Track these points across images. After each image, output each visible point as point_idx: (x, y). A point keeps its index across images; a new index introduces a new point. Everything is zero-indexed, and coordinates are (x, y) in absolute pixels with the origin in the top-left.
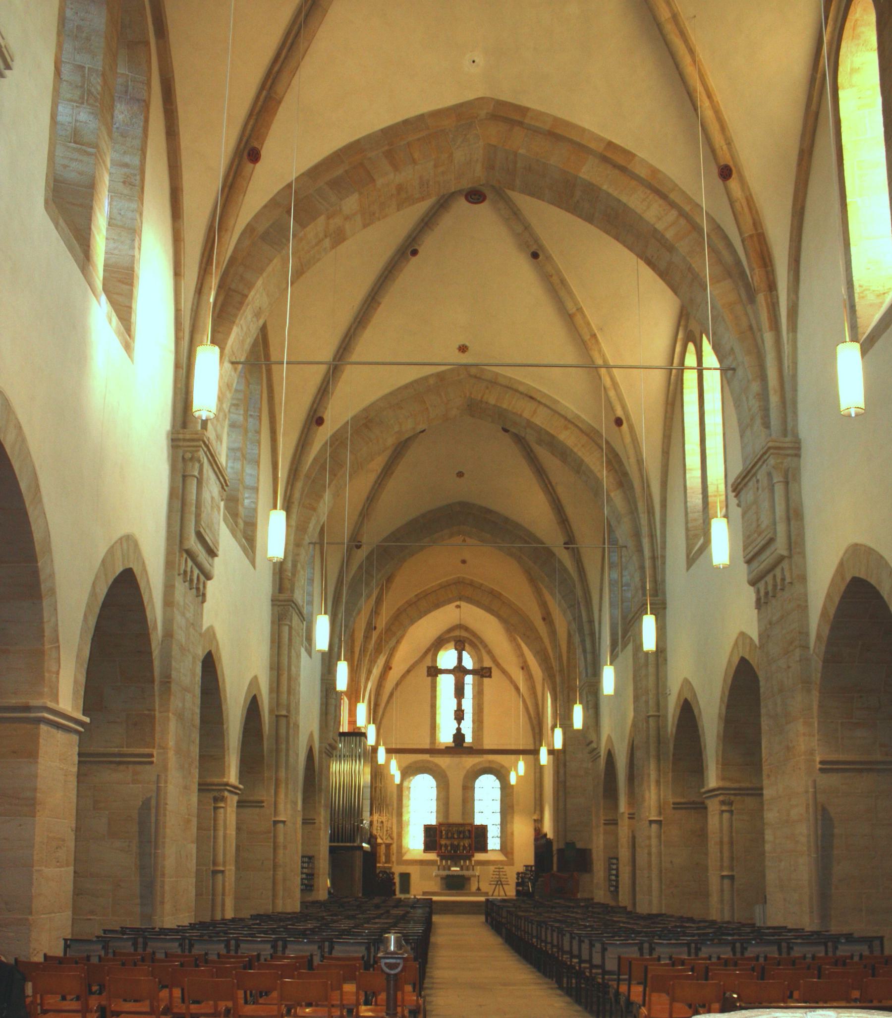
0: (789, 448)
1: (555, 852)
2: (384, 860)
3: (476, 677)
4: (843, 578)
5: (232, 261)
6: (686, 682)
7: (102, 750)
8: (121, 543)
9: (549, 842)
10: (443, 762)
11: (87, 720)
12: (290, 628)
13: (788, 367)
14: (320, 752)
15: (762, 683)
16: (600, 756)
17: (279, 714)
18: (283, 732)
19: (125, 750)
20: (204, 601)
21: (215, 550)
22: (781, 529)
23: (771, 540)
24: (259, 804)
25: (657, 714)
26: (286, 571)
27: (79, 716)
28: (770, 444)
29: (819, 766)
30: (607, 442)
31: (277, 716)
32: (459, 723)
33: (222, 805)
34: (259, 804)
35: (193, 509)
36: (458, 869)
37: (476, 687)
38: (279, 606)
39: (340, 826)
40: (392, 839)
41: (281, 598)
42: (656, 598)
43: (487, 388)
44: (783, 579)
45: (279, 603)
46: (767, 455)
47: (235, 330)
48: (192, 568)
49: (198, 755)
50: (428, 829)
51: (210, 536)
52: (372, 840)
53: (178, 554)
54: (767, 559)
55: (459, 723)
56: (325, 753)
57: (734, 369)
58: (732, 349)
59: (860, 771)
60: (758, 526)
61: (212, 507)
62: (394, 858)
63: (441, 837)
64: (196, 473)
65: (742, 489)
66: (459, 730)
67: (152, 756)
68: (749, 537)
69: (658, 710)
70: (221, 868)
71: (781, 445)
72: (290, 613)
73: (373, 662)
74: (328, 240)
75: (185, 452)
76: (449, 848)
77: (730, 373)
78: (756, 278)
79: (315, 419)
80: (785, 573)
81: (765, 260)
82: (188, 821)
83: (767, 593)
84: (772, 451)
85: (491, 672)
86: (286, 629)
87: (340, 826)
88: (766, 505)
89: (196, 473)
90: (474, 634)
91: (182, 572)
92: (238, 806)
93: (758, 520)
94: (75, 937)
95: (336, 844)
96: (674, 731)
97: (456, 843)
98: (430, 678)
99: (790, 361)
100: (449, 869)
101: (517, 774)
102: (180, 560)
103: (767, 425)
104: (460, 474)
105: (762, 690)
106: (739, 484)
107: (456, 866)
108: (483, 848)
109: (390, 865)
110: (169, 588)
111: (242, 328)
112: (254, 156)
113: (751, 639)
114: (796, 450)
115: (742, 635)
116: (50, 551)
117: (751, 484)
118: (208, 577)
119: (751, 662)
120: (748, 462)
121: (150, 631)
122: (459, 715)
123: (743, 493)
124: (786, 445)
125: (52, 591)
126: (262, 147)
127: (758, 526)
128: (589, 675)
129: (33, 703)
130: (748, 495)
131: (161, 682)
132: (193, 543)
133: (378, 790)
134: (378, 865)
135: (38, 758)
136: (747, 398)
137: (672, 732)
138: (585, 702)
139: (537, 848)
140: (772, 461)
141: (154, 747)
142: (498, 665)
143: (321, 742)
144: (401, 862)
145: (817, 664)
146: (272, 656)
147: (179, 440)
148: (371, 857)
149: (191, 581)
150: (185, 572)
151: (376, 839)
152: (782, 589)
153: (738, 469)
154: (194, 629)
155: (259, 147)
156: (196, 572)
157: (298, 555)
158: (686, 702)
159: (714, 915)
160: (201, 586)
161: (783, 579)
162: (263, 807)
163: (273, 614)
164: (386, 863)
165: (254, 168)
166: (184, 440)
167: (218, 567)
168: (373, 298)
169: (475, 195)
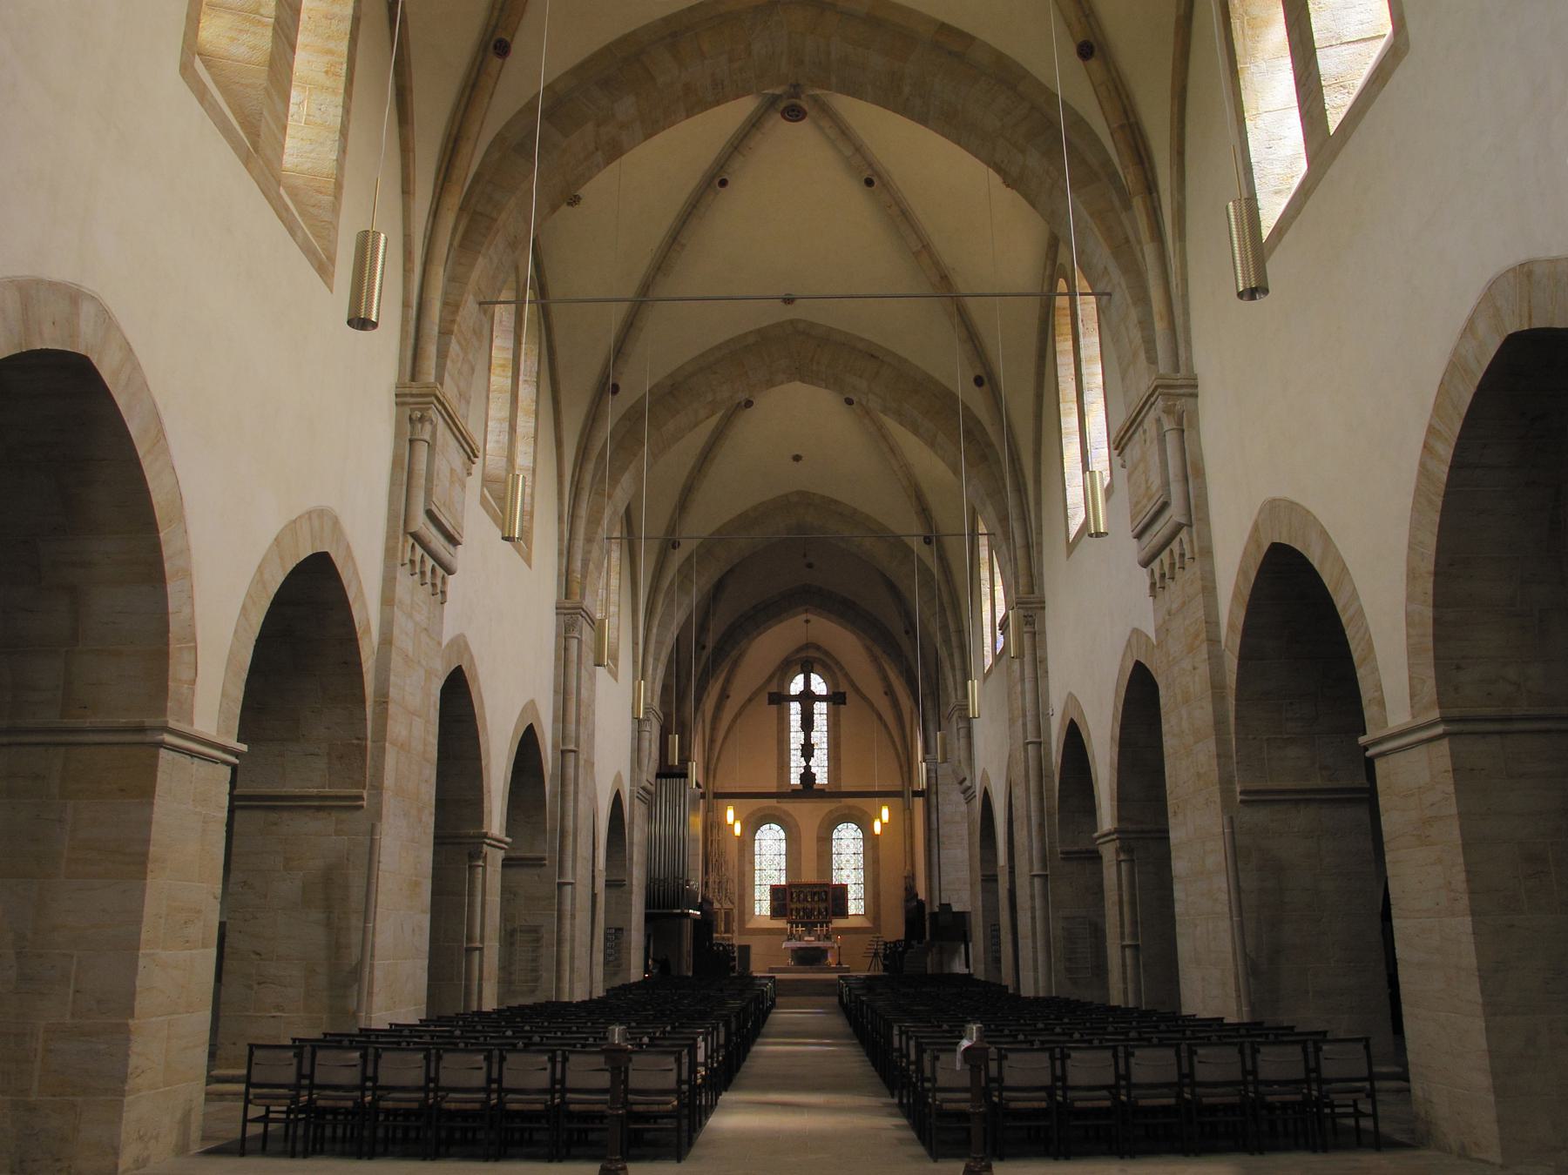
0: (1181, 386)
1: (927, 917)
2: (723, 929)
4: (1259, 546)
5: (478, 177)
7: (297, 791)
8: (310, 518)
9: (921, 904)
10: (789, 806)
11: (244, 748)
12: (580, 641)
13: (1177, 285)
14: (631, 797)
15: (1162, 692)
16: (975, 796)
17: (565, 748)
18: (571, 771)
19: (327, 791)
21: (457, 536)
22: (1176, 490)
23: (1165, 506)
24: (537, 862)
25: (1038, 740)
26: (574, 571)
27: (232, 742)
28: (1160, 382)
29: (1239, 798)
30: (966, 408)
31: (563, 752)
32: (808, 761)
33: (480, 863)
34: (537, 862)
35: (423, 481)
36: (813, 939)
37: (832, 719)
39: (661, 888)
40: (733, 903)
41: (567, 605)
42: (1032, 596)
43: (819, 346)
44: (1182, 555)
45: (566, 611)
46: (1155, 396)
47: (481, 262)
48: (422, 556)
49: (434, 798)
50: (775, 890)
51: (447, 515)
52: (702, 906)
53: (401, 538)
54: (1161, 529)
55: (808, 761)
56: (637, 797)
57: (1109, 294)
58: (1105, 268)
59: (1297, 802)
60: (1148, 488)
61: (452, 483)
62: (735, 926)
63: (791, 901)
64: (427, 437)
65: (1126, 444)
67: (361, 798)
68: (1137, 503)
69: (1039, 734)
70: (478, 945)
71: (1171, 382)
72: (579, 623)
73: (702, 689)
74: (600, 153)
75: (412, 410)
76: (801, 913)
77: (1105, 298)
78: (1129, 177)
80: (1185, 546)
81: (1140, 154)
82: (417, 884)
83: (1163, 576)
84: (1159, 390)
85: (845, 698)
86: (574, 643)
87: (661, 888)
88: (1155, 460)
90: (827, 653)
91: (407, 561)
92: (503, 866)
93: (1147, 481)
94: (429, 1018)
95: (652, 911)
96: (1060, 761)
97: (809, 906)
98: (774, 707)
99: (1179, 278)
101: (881, 821)
102: (403, 546)
103: (1152, 360)
105: (1162, 701)
106: (1122, 438)
107: (809, 935)
108: (842, 911)
109: (730, 935)
110: (389, 582)
111: (491, 259)
112: (502, 49)
113: (1147, 636)
114: (1191, 389)
115: (1135, 631)
116: (181, 518)
117: (1137, 436)
119: (1147, 666)
120: (1132, 408)
121: (359, 636)
122: (808, 750)
123: (1127, 451)
124: (1179, 382)
125: (186, 573)
126: (512, 40)
127: (1148, 488)
128: (959, 697)
129: (149, 722)
130: (1134, 451)
131: (375, 702)
132: (420, 523)
133: (715, 845)
134: (715, 935)
135: (153, 798)
136: (1127, 328)
137: (1057, 762)
139: (908, 912)
140: (1160, 404)
141: (364, 788)
142: (857, 690)
143: (632, 785)
144: (744, 931)
145: (1231, 663)
146: (556, 676)
147: (405, 395)
148: (705, 926)
149: (423, 573)
150: (412, 562)
151: (712, 904)
153: (1121, 419)
154: (429, 636)
155: (508, 39)
156: (430, 562)
157: (589, 552)
158: (1072, 721)
159: (1116, 999)
160: (439, 582)
161: (1182, 555)
162: (545, 865)
163: (558, 626)
164: (725, 932)
165: (503, 64)
166: (412, 395)
167: (461, 558)
168: (675, 239)
169: (793, 110)
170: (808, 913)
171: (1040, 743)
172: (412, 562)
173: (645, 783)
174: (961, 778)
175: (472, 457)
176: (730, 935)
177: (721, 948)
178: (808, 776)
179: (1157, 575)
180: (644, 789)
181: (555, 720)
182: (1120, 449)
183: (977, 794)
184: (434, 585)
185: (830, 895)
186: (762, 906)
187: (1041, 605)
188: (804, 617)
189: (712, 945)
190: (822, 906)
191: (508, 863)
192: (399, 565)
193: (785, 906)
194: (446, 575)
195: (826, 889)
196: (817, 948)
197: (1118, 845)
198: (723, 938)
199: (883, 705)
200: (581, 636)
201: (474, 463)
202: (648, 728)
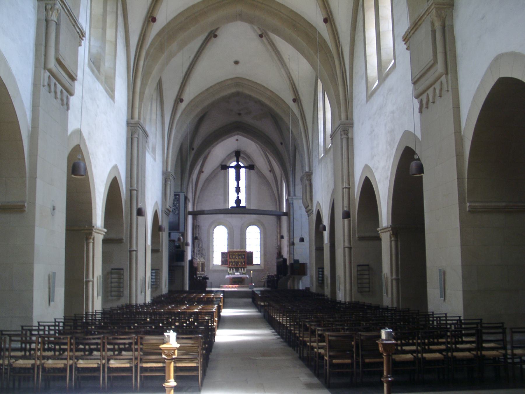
3: (247, 169)
6: (367, 167)
9: (285, 260)
16: (313, 214)
20: (68, 109)
25: (349, 186)
32: (238, 194)
38: (131, 126)
50: (223, 254)
55: (238, 194)
56: (165, 213)
64: (55, 19)
66: (238, 197)
76: (234, 264)
79: (151, 19)
89: (55, 19)
91: (46, 84)
100: (234, 274)
104: (236, 63)
107: (237, 272)
118: (71, 94)
122: (238, 190)
134: (198, 273)
138: (180, 348)
149: (55, 92)
152: (434, 102)
156: (59, 87)
167: (78, 87)
170: (237, 263)
171: (349, 188)
172: (49, 85)
173: (168, 207)
174: (307, 206)
175: (82, 37)
176: (203, 273)
177: (201, 278)
178: (238, 201)
179: (424, 102)
180: (167, 209)
181: (127, 177)
182: (406, 40)
183: (314, 212)
184: (62, 100)
185: (246, 256)
186: (217, 260)
187: (352, 125)
188: (236, 137)
189: (197, 277)
190: (242, 260)
191: (105, 241)
192: (42, 86)
193: (227, 260)
194: (69, 96)
195: (244, 253)
196: (241, 278)
197: (391, 233)
198: (201, 274)
199: (269, 175)
200: (139, 137)
201: (82, 40)
202: (169, 183)
